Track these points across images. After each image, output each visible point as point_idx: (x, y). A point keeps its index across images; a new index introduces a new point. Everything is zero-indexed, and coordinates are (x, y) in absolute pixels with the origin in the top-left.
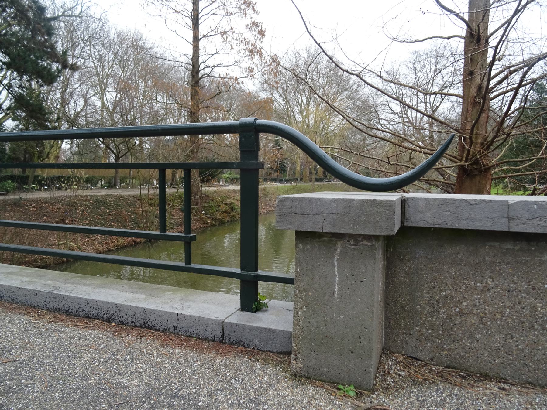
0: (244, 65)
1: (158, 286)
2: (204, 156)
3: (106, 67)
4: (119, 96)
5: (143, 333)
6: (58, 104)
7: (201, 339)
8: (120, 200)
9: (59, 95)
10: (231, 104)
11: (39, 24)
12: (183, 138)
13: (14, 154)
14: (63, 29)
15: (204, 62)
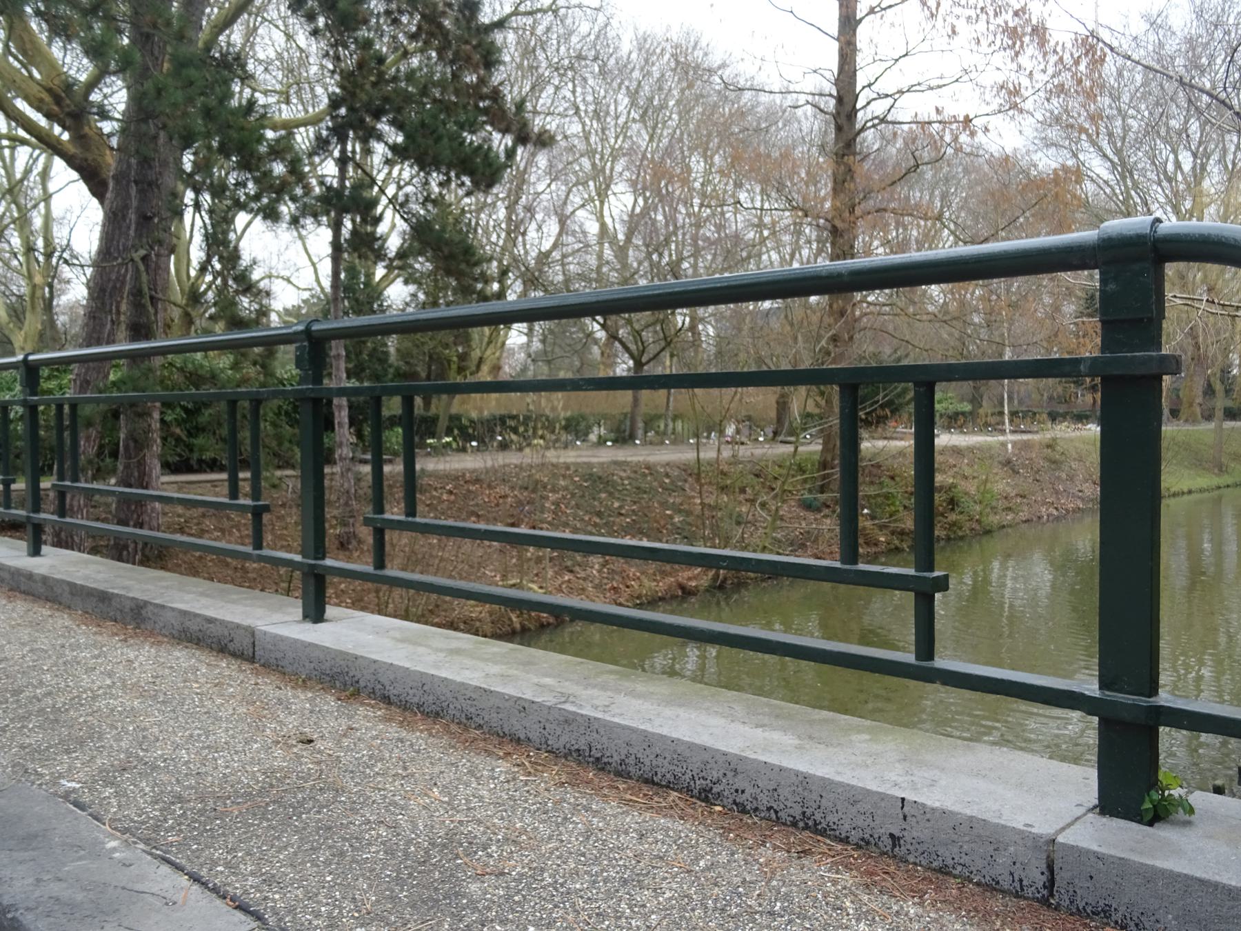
0: (991, 78)
1: (825, 714)
2: (868, 350)
3: (611, 134)
4: (641, 201)
5: (803, 842)
6: (499, 236)
7: (978, 884)
8: (645, 475)
9: (502, 213)
10: (944, 197)
11: (467, 42)
12: (807, 302)
13: (407, 363)
14: (512, 50)
15: (869, 85)
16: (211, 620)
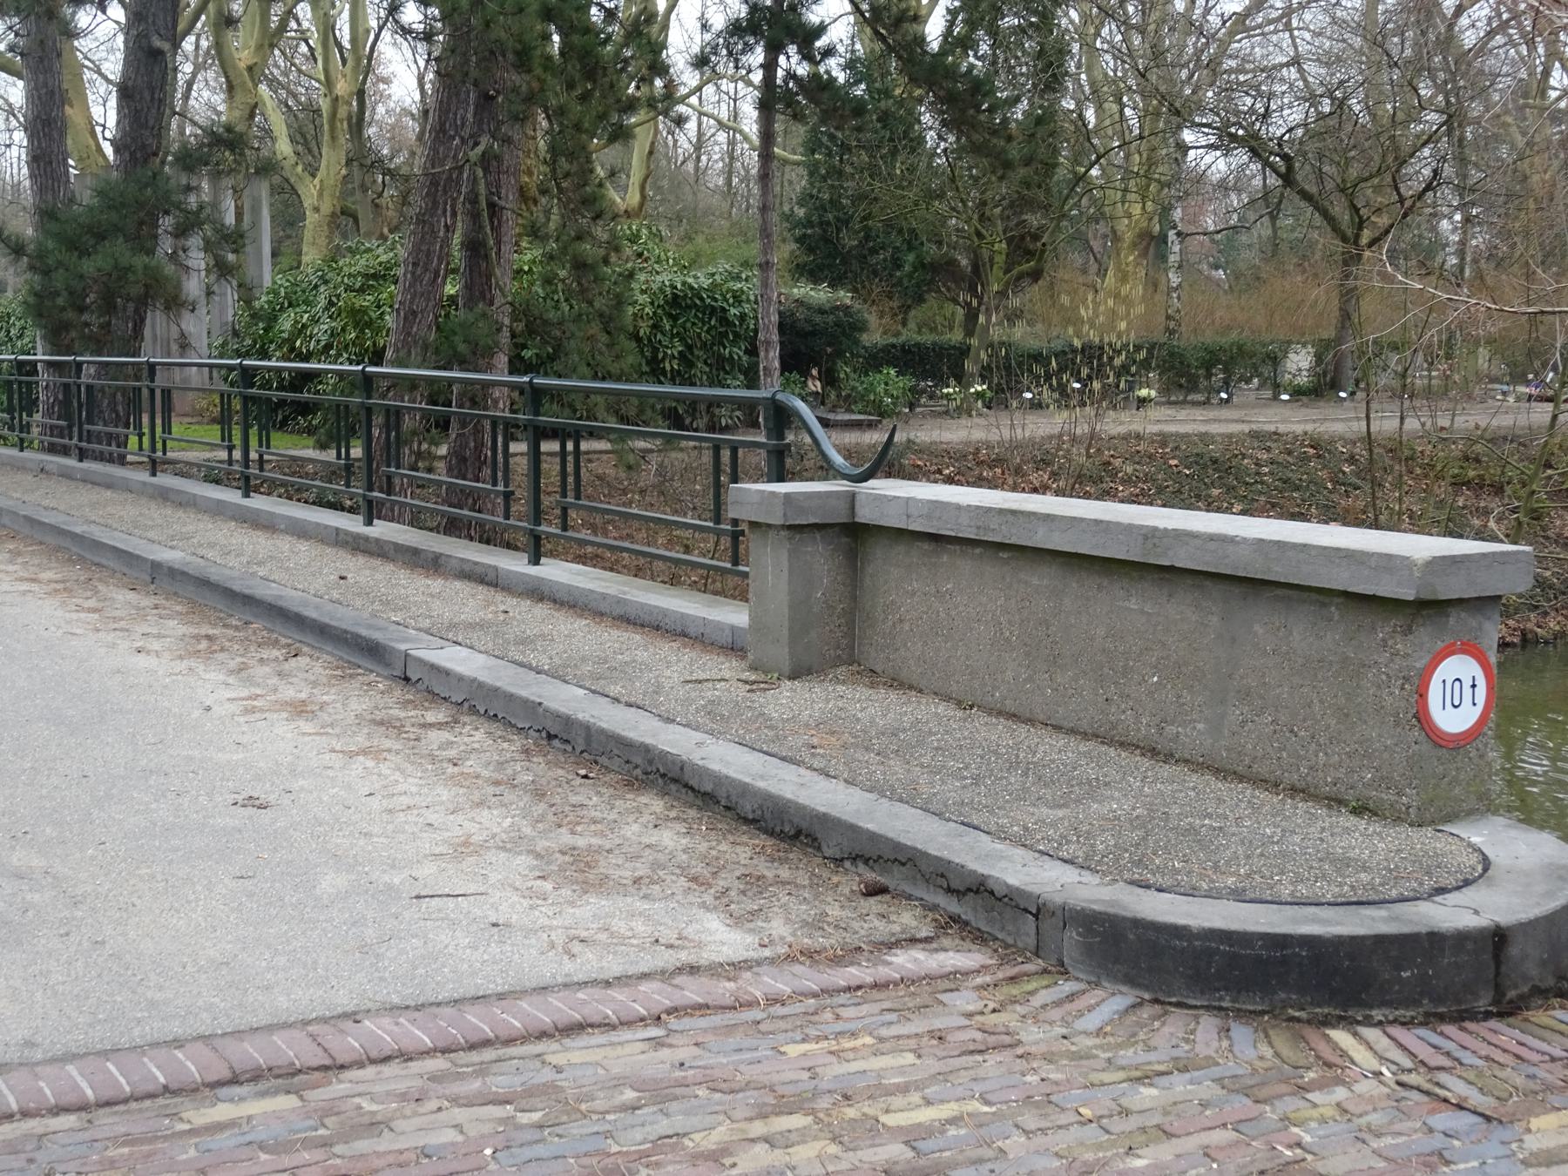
8: (1305, 458)
16: (476, 563)
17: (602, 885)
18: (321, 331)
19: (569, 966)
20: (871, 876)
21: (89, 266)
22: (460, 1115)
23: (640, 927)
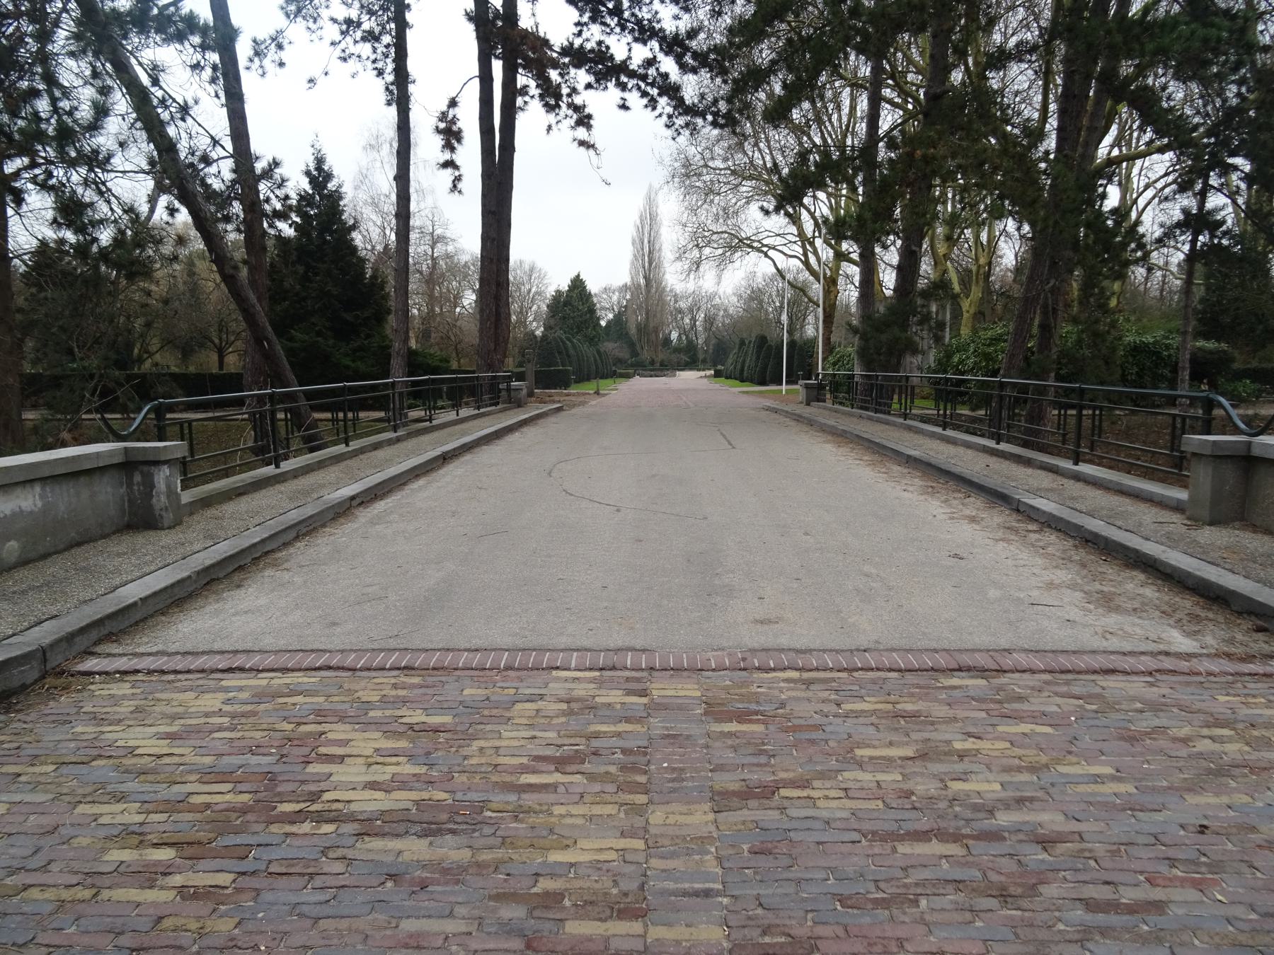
17: (1117, 609)
18: (971, 362)
19: (1105, 644)
20: (1260, 623)
21: (884, 337)
22: (1058, 700)
23: (1138, 631)
